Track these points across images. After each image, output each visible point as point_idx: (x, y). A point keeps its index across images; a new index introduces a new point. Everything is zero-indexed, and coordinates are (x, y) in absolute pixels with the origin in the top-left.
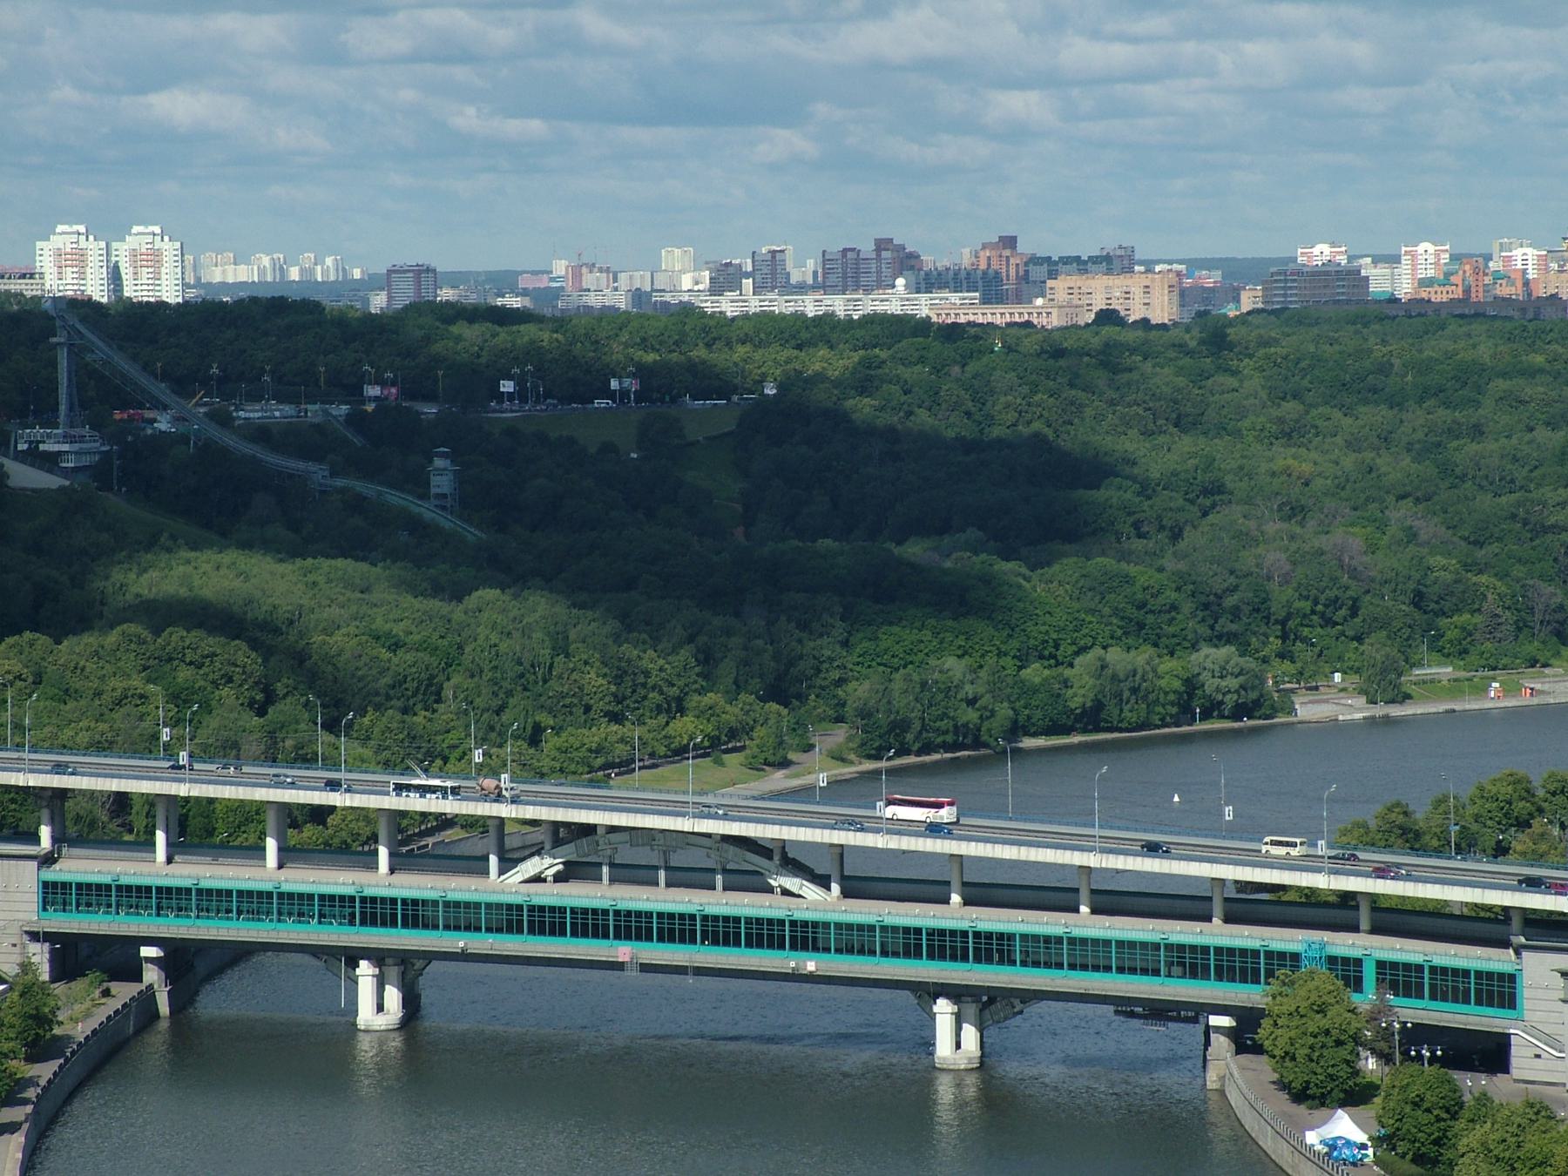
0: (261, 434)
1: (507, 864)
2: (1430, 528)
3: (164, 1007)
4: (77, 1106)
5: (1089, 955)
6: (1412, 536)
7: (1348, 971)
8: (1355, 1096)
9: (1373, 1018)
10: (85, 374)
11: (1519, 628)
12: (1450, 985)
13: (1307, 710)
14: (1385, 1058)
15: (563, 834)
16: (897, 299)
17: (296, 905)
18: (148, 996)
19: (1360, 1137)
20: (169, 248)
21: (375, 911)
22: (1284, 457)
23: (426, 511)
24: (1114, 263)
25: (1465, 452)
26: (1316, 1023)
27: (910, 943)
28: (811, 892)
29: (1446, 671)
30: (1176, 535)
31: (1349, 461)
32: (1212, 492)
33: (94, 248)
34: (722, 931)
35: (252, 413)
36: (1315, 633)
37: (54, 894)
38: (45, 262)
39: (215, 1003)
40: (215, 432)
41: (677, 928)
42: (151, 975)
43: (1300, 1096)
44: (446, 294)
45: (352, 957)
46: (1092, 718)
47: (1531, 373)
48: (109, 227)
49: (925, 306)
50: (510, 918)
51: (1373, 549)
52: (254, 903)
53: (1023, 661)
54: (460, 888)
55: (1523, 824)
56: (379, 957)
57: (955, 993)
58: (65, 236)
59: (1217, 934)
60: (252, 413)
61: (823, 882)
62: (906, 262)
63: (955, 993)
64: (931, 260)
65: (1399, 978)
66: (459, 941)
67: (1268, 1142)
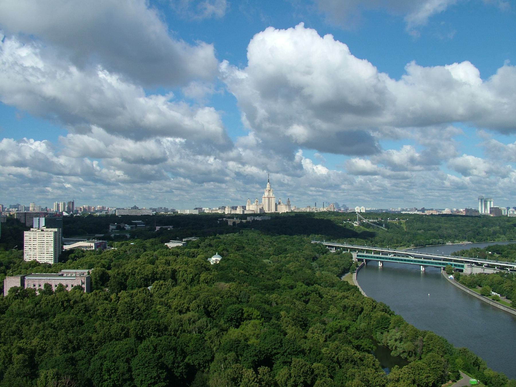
0: (371, 222)
1: (390, 255)
2: (456, 231)
3: (365, 264)
4: (360, 270)
5: (432, 263)
6: (455, 231)
7: (452, 265)
8: (452, 274)
9: (454, 268)
10: (359, 218)
11: (463, 238)
12: (459, 266)
13: (447, 244)
14: (454, 271)
15: (393, 253)
16: (416, 212)
17: (374, 257)
18: (364, 263)
19: (453, 277)
20: (364, 208)
21: (381, 258)
22: (445, 225)
23: (383, 228)
24: (432, 210)
25: (458, 225)
26: (450, 269)
27: (419, 262)
28: (412, 258)
29: (457, 241)
30: (437, 231)
31: (450, 225)
32: (440, 228)
33: (359, 208)
34: (405, 260)
35: (370, 221)
36: (448, 238)
37: (358, 256)
38: (356, 209)
39: (369, 264)
40: (368, 222)
41: (402, 260)
42: (364, 262)
43: (448, 274)
44: (384, 211)
45: (378, 261)
46: (432, 244)
47: (463, 219)
48: (360, 207)
49: (418, 213)
50: (390, 259)
51: (452, 232)
52: (372, 257)
53: (426, 240)
54: (386, 256)
55: (464, 253)
56: (380, 261)
57: (422, 265)
58: (357, 207)
59: (442, 262)
60: (370, 221)
61: (413, 257)
62: (416, 209)
63: (422, 265)
64: (418, 209)
65: (455, 265)
66: (386, 260)
67: (446, 277)
